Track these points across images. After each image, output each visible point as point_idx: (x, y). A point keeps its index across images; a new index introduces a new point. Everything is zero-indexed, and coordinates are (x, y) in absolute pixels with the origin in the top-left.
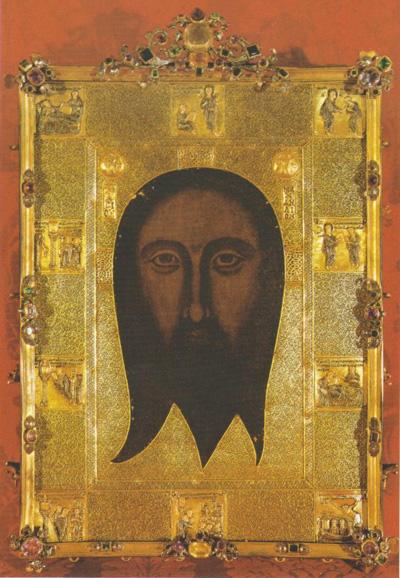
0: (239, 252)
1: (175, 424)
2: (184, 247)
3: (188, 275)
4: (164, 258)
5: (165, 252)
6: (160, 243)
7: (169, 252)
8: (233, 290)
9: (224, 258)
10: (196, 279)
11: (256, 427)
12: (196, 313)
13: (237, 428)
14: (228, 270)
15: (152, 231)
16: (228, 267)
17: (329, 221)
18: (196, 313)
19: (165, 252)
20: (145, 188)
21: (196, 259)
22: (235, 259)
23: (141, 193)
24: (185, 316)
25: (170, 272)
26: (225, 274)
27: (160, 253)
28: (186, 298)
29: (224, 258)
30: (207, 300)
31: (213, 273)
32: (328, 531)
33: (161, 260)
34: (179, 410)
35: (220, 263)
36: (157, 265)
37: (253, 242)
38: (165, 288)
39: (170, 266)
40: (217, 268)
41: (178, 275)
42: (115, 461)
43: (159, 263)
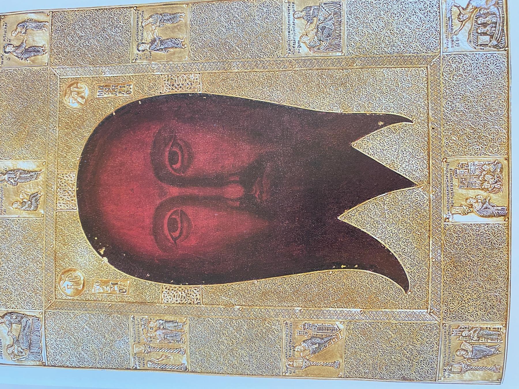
0: (166, 145)
1: (367, 217)
2: (161, 204)
3: (192, 200)
4: (172, 224)
5: (166, 226)
6: (156, 231)
7: (166, 221)
8: (208, 151)
9: (173, 160)
10: (194, 191)
11: (367, 124)
12: (234, 192)
13: (369, 146)
14: (186, 156)
15: (146, 244)
16: (183, 156)
17: (135, 47)
18: (234, 192)
19: (166, 226)
20: (97, 248)
21: (175, 191)
22: (175, 149)
23: (102, 252)
24: (238, 204)
25: (189, 220)
26: (191, 157)
27: (166, 232)
28: (216, 202)
29: (173, 160)
30: (220, 181)
31: (190, 172)
32: (492, 37)
33: (176, 163)
34: (346, 212)
35: (178, 166)
36: (180, 236)
37: (155, 128)
38: (206, 225)
39: (182, 222)
40: (185, 168)
41: (190, 210)
42: (406, 287)
43: (178, 233)
